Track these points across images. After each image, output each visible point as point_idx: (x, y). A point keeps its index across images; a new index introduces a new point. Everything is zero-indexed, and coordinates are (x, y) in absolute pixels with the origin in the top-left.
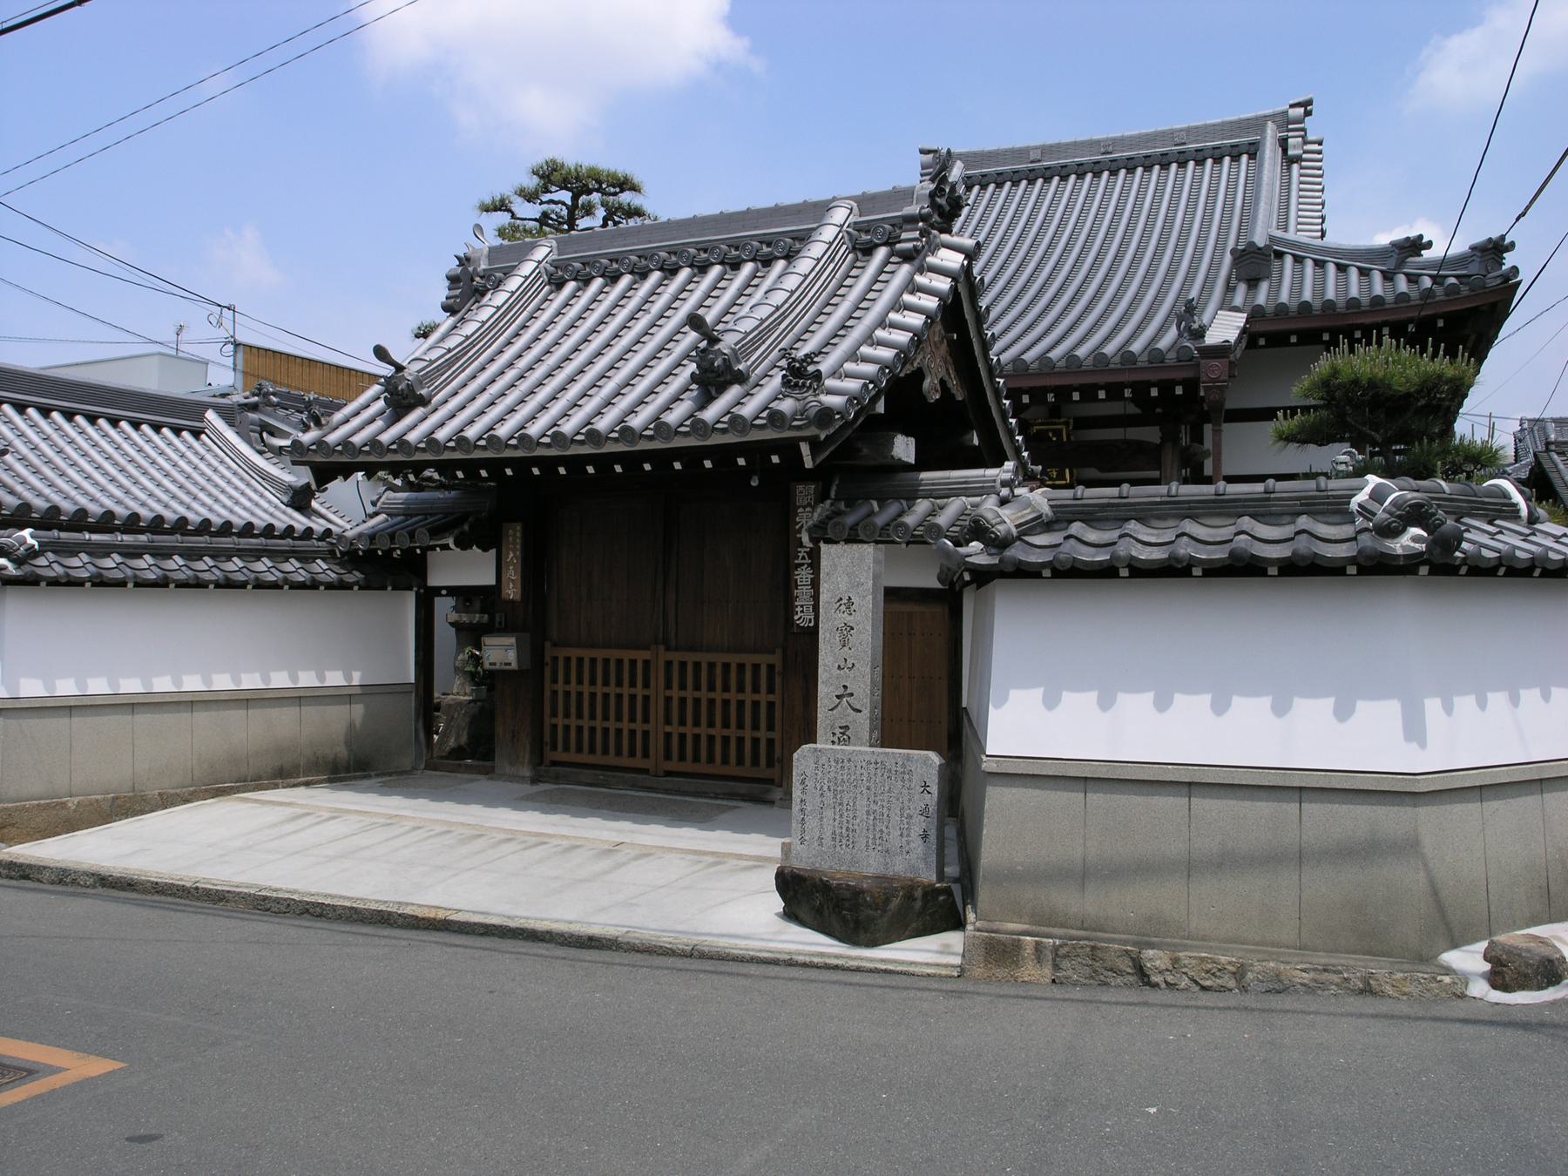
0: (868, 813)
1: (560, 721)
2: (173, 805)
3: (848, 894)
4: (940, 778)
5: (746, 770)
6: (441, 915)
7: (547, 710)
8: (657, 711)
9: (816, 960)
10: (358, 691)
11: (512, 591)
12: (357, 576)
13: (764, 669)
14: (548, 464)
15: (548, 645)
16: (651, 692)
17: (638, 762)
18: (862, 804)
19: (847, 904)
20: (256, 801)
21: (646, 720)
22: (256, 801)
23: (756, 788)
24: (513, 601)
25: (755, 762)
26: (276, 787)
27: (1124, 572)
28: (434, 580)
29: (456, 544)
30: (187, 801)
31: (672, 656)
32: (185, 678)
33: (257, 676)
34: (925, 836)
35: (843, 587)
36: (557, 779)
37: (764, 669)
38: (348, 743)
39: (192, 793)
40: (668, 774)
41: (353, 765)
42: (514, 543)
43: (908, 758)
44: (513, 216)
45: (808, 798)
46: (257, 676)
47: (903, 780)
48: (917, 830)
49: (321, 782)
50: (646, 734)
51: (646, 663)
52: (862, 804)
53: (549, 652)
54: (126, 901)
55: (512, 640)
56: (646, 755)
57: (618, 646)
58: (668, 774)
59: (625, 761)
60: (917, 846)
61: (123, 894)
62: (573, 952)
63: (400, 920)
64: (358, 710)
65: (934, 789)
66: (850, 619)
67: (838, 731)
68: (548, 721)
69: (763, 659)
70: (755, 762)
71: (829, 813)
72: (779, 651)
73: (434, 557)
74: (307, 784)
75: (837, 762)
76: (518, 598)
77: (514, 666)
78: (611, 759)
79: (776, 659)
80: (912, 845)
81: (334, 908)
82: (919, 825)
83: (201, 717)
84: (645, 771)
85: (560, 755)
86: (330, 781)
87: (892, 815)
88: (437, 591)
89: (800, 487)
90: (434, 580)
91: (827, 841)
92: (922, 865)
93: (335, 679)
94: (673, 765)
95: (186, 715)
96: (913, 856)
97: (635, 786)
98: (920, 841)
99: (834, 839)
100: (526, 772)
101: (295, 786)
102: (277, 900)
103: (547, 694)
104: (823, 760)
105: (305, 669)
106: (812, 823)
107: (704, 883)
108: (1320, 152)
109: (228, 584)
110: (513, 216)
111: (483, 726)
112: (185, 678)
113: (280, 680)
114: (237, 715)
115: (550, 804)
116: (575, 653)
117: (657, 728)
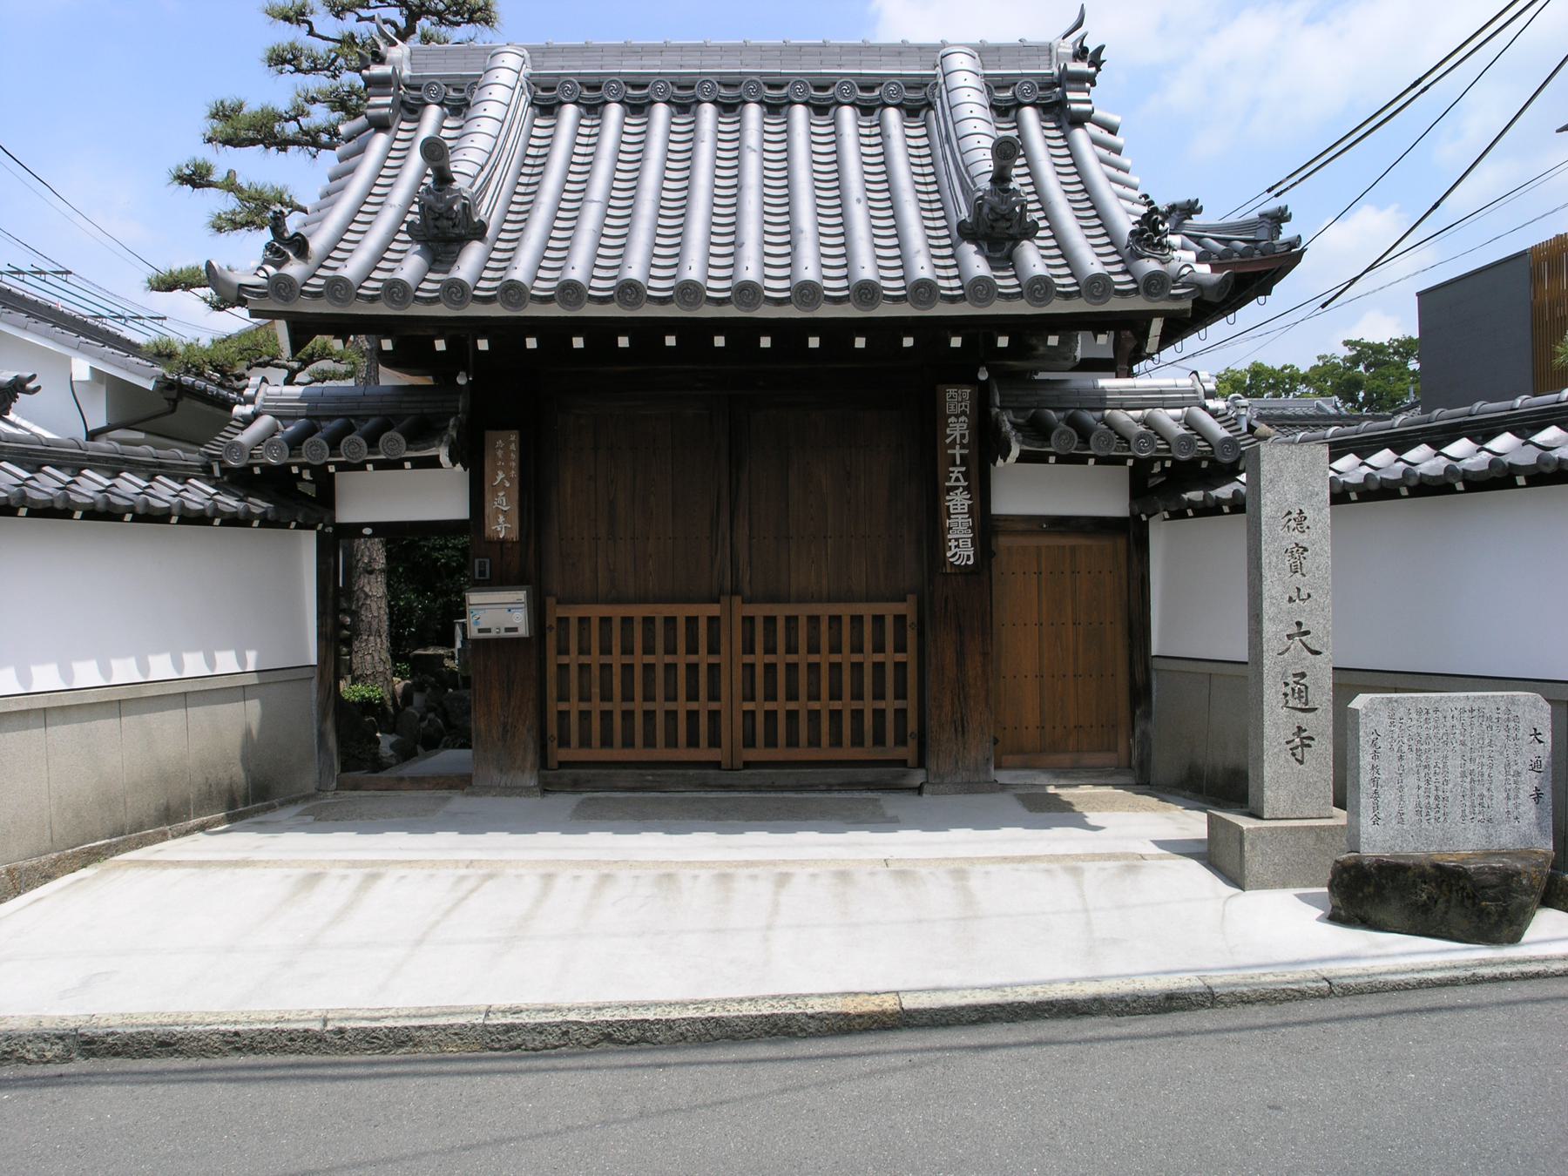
0: (1463, 775)
1: (574, 706)
2: (29, 886)
3: (1494, 880)
4: (1554, 722)
5: (868, 752)
6: (889, 1004)
7: (552, 690)
8: (731, 682)
9: (1508, 970)
10: (253, 679)
11: (503, 524)
12: (259, 505)
13: (889, 622)
14: (837, 331)
15: (551, 601)
16: (721, 659)
17: (704, 753)
18: (1454, 764)
19: (1491, 892)
20: (149, 864)
21: (714, 696)
22: (149, 864)
23: (886, 773)
24: (503, 542)
25: (879, 740)
26: (164, 837)
27: (1460, 486)
28: (347, 513)
29: (454, 459)
30: (48, 877)
31: (750, 610)
32: (35, 670)
33: (132, 662)
34: (1538, 796)
35: (1292, 498)
36: (576, 786)
37: (889, 622)
38: (245, 760)
39: (55, 863)
40: (747, 765)
41: (255, 796)
42: (506, 458)
43: (1513, 701)
44: (311, 32)
45: (1381, 763)
46: (132, 662)
47: (1507, 729)
48: (1527, 789)
49: (219, 823)
50: (714, 716)
51: (713, 621)
52: (1454, 764)
53: (556, 611)
54: (159, 1076)
55: (521, 595)
56: (715, 742)
57: (673, 600)
58: (747, 765)
59: (683, 753)
60: (1529, 811)
61: (148, 1064)
62: (1144, 1025)
63: (813, 1025)
64: (251, 712)
65: (1547, 737)
66: (1302, 539)
67: (1291, 680)
68: (554, 706)
69: (889, 609)
70: (879, 740)
71: (1411, 780)
72: (911, 598)
73: (346, 483)
74: (202, 828)
75: (1419, 712)
76: (515, 536)
77: (523, 631)
78: (661, 753)
79: (907, 608)
80: (1522, 808)
81: (669, 1024)
82: (1530, 782)
83: (61, 733)
84: (716, 765)
85: (574, 753)
86: (231, 819)
87: (1494, 773)
88: (354, 530)
89: (951, 391)
90: (347, 513)
91: (1410, 815)
92: (1535, 832)
93: (227, 662)
94: (759, 753)
95: (37, 733)
96: (1524, 822)
97: (705, 786)
98: (1532, 803)
99: (1419, 813)
100: (530, 779)
101: (188, 832)
102: (539, 1029)
103: (552, 670)
104: (1401, 712)
105: (192, 649)
106: (1388, 795)
107: (1079, 894)
108: (1089, 102)
109: (104, 513)
110: (311, 32)
111: (392, 723)
112: (35, 670)
113: (161, 668)
114: (106, 726)
115: (584, 819)
116: (595, 612)
117: (732, 706)
